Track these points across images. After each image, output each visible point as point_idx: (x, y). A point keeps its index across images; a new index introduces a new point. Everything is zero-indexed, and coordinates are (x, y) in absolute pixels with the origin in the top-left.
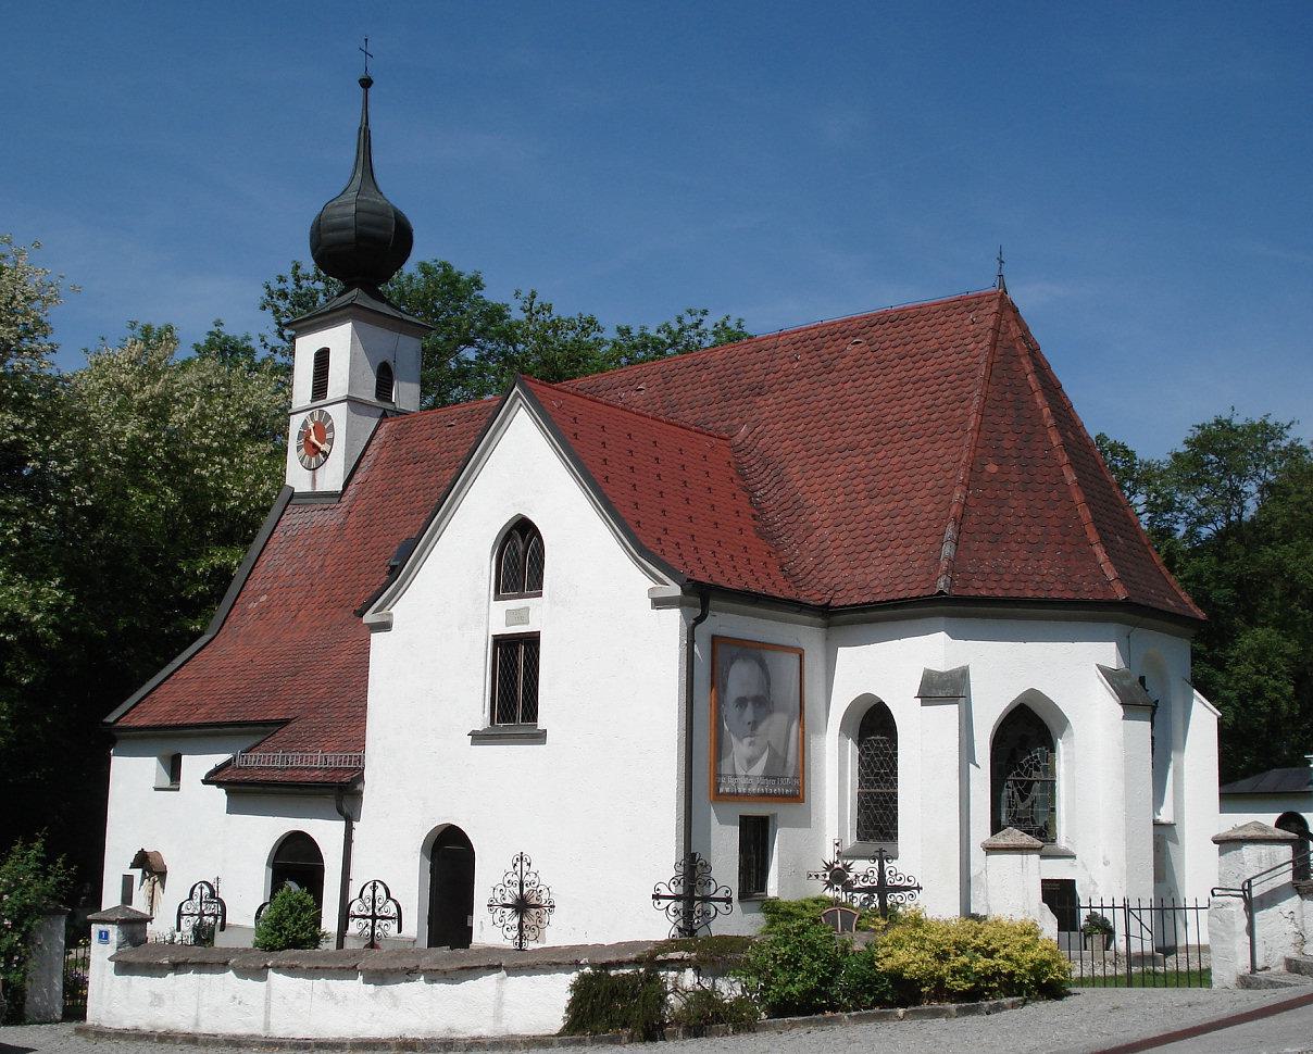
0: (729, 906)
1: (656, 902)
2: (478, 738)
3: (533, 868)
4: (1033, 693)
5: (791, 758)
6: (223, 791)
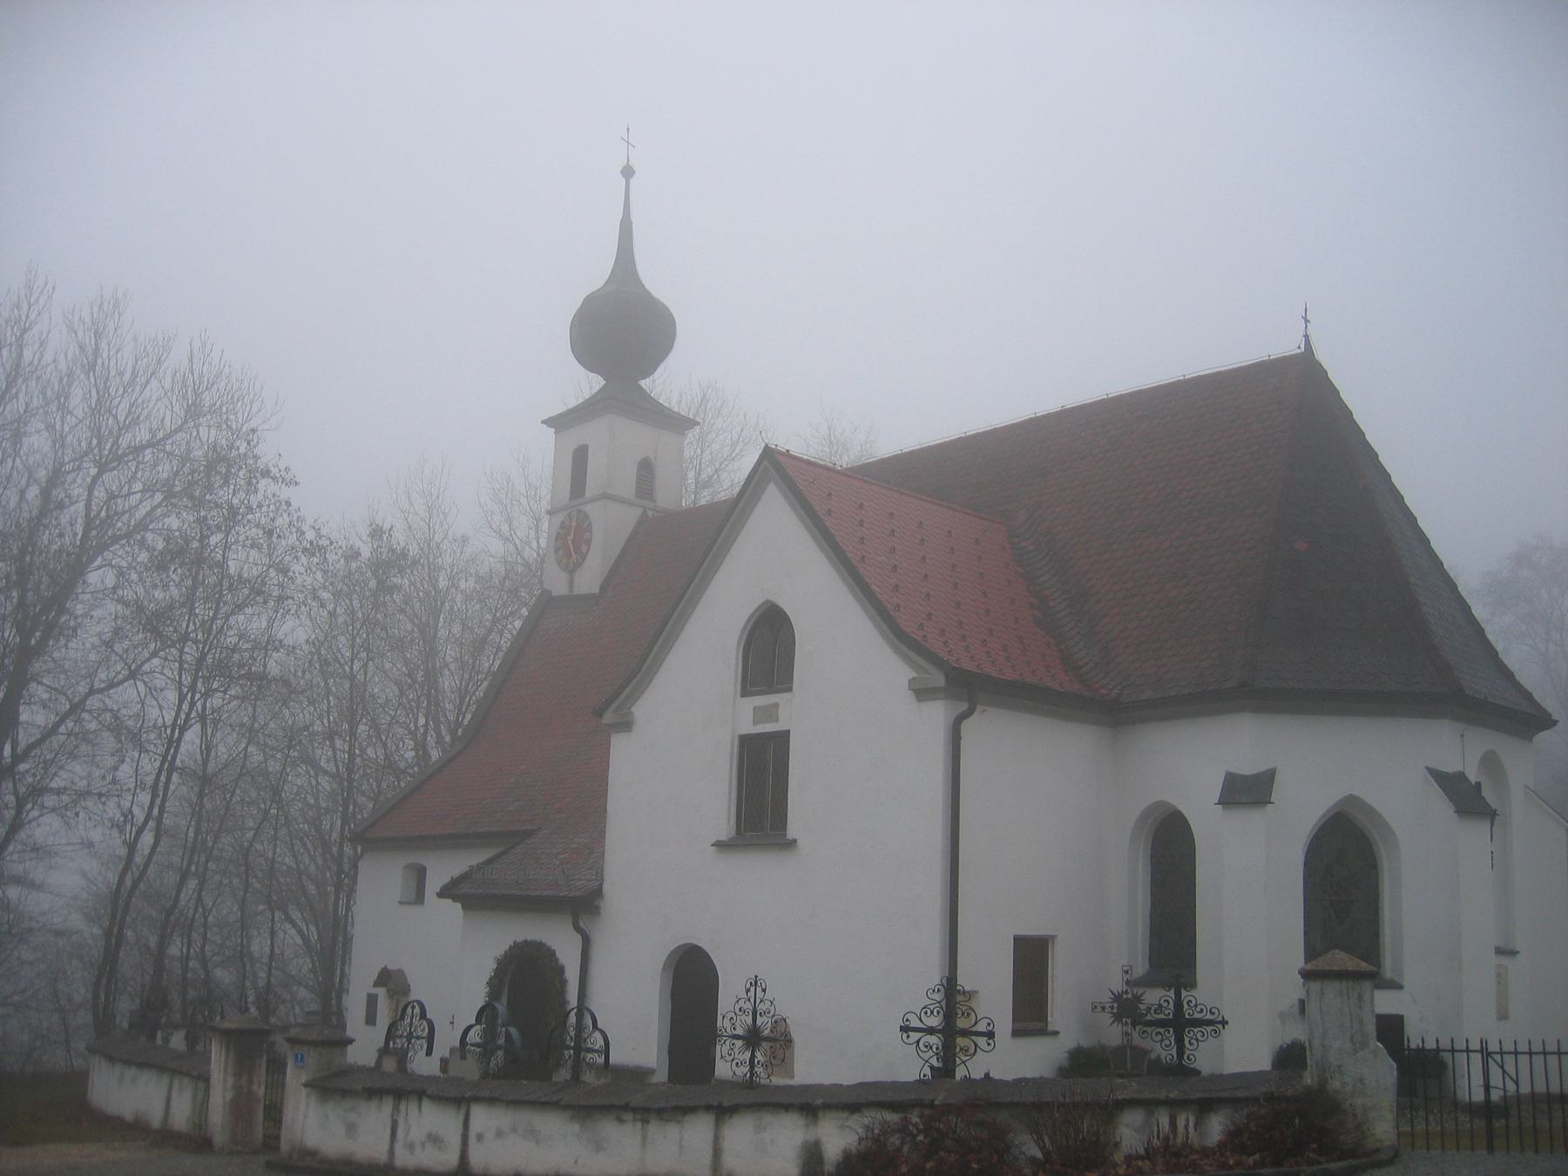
0: (991, 1041)
1: (905, 1035)
2: (720, 845)
3: (769, 996)
4: (1351, 800)
5: (88, 343)
6: (459, 906)
